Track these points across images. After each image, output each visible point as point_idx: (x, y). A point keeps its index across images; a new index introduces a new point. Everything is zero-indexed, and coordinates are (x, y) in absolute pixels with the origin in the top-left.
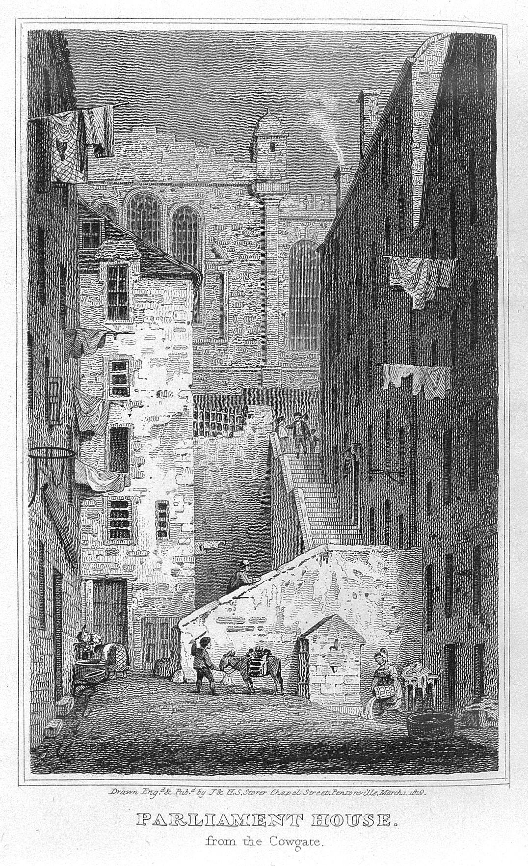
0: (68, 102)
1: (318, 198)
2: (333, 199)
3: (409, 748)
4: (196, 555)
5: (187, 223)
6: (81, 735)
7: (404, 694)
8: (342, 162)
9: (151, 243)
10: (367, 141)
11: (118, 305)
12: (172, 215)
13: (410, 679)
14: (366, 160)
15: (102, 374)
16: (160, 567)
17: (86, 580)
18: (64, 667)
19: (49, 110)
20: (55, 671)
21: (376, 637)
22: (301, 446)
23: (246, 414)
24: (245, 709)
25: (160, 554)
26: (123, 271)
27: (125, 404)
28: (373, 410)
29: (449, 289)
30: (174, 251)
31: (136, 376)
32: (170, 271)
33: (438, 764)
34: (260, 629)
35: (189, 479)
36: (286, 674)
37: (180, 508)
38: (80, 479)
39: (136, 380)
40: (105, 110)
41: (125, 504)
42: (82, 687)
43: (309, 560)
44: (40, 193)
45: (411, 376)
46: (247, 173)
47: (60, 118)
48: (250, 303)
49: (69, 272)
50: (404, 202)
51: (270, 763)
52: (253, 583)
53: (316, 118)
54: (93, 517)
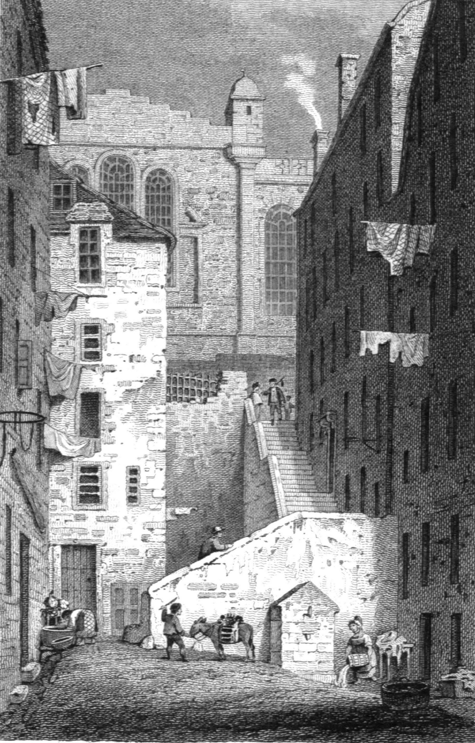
0: (41, 63)
1: (295, 162)
2: (310, 164)
3: (383, 716)
4: (167, 521)
5: (161, 187)
6: (47, 702)
7: (378, 662)
8: (319, 126)
9: (122, 205)
10: (345, 106)
11: (90, 269)
12: (145, 178)
13: (385, 647)
14: (344, 125)
15: (74, 338)
16: (129, 533)
17: (55, 545)
18: (30, 634)
19: (20, 72)
20: (21, 636)
21: (350, 606)
22: (276, 414)
23: (221, 380)
24: (215, 676)
25: (130, 520)
26: (95, 234)
27: (97, 369)
28: (350, 376)
29: (427, 255)
30: (147, 214)
31: (108, 340)
32: (142, 235)
33: (412, 733)
34: (232, 595)
35: (161, 444)
36: (258, 640)
37: (150, 474)
38: (49, 443)
39: (108, 344)
40: (78, 72)
41: (95, 469)
42: (49, 653)
43: (282, 528)
44: (10, 154)
45: (388, 344)
46: (222, 136)
47: (33, 79)
48: (225, 267)
49: (40, 235)
50: (382, 170)
51: (239, 730)
52: (225, 549)
53: (294, 81)
54: (64, 481)
